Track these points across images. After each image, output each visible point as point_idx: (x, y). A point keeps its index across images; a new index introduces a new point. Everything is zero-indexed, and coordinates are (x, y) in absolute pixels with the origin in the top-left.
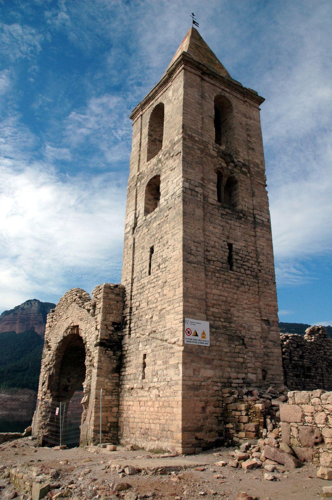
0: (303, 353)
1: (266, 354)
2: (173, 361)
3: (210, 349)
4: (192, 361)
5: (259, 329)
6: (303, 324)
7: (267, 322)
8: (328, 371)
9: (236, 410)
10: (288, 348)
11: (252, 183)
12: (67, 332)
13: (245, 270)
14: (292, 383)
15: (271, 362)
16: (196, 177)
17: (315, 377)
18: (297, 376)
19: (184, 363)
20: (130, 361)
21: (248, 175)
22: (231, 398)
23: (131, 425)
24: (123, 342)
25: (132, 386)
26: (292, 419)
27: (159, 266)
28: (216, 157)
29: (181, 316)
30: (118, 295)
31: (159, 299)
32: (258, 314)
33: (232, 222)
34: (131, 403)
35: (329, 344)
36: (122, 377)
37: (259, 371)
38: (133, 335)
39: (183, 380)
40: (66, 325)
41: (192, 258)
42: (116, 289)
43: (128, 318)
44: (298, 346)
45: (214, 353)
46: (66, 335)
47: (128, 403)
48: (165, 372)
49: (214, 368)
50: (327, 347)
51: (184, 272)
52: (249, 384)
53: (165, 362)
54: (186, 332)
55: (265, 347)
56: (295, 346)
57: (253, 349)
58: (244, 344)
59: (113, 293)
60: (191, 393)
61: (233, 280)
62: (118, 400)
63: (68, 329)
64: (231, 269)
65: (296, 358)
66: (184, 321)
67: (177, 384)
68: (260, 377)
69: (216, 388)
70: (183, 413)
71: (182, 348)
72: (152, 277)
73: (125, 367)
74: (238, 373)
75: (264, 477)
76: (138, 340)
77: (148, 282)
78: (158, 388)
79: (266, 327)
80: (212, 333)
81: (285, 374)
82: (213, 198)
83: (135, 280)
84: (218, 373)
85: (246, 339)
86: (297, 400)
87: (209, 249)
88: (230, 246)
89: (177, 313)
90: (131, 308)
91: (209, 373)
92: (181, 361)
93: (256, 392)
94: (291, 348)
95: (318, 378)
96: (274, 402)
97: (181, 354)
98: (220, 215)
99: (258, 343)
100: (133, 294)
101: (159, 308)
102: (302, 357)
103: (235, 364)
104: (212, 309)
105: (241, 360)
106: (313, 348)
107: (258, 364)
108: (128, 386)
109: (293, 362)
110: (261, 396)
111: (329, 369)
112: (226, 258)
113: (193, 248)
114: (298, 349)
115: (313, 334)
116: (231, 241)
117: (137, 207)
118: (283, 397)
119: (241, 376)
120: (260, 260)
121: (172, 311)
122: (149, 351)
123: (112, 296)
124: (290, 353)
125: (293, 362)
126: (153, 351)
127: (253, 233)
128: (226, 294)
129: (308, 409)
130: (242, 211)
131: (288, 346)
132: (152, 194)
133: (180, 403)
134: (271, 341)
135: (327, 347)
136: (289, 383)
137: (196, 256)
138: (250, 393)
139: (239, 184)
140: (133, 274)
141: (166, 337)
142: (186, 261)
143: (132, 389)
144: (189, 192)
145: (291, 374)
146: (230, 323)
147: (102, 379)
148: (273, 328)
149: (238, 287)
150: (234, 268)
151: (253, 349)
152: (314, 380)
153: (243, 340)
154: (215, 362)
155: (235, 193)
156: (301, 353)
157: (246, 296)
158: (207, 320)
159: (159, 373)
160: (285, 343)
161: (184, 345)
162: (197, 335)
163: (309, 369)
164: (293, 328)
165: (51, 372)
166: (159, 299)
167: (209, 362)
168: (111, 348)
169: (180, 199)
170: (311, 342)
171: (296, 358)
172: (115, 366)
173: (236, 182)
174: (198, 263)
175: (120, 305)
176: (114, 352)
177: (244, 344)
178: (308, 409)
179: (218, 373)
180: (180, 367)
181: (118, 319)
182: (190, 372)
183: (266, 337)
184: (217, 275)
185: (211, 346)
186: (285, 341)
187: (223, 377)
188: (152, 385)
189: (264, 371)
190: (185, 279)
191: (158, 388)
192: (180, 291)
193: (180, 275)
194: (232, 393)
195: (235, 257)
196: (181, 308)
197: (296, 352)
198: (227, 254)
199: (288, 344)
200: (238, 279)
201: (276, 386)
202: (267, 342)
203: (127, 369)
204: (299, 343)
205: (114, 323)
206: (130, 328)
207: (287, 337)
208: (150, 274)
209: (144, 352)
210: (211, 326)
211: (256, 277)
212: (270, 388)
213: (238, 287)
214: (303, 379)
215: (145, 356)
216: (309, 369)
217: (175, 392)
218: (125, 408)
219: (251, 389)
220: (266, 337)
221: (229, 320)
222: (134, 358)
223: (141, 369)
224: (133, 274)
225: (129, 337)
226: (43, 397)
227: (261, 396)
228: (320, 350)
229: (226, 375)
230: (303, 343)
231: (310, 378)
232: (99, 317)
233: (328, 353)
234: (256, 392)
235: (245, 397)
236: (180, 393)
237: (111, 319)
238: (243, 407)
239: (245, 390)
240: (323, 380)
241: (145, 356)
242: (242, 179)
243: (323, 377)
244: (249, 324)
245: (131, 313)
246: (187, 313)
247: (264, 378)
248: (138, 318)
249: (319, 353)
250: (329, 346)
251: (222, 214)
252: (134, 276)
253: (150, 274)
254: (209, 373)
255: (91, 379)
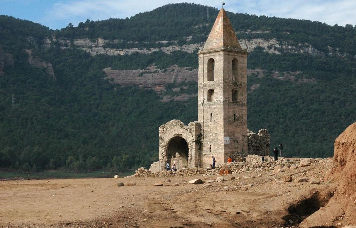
0: (256, 141)
1: (243, 145)
2: (221, 147)
3: (229, 144)
4: (226, 148)
5: (242, 138)
6: (309, 21)
7: (244, 136)
8: (267, 148)
9: (236, 159)
10: (251, 139)
11: (242, 91)
12: (174, 136)
13: (239, 121)
14: (251, 153)
15: (244, 147)
16: (226, 96)
17: (261, 150)
18: (254, 150)
19: (224, 148)
20: (204, 147)
21: (241, 88)
22: (235, 157)
23: (206, 164)
24: (201, 141)
25: (206, 154)
26: (248, 161)
27: (215, 120)
28: (232, 86)
29: (223, 137)
30: (198, 126)
31: (215, 130)
32: (242, 134)
33: (236, 107)
34: (206, 158)
35: (269, 137)
36: (201, 151)
37: (241, 150)
38: (205, 139)
39: (224, 152)
40: (174, 133)
41: (225, 121)
42: (198, 124)
43: (202, 133)
44: (255, 138)
45: (230, 145)
46: (174, 137)
47: (204, 158)
48: (218, 150)
49: (230, 149)
50: (268, 138)
51: (224, 125)
52: (238, 153)
53: (218, 148)
54: (224, 140)
55: (243, 143)
56: (253, 138)
57: (240, 144)
58: (237, 143)
59: (197, 126)
60: (226, 155)
61: (235, 125)
62: (200, 158)
63: (175, 135)
64: (235, 122)
65: (253, 143)
66: (224, 138)
67: (222, 153)
68: (241, 151)
69: (231, 154)
70: (224, 160)
71: (223, 145)
72: (212, 123)
73: (202, 148)
74: (236, 150)
75: (264, 77)
76: (208, 141)
77: (210, 124)
78: (216, 154)
79: (243, 137)
80: (230, 140)
81: (249, 149)
82: (231, 101)
83: (204, 122)
84: (231, 150)
85: (238, 141)
86: (250, 157)
87: (230, 117)
88: (235, 114)
89: (222, 136)
90: (203, 131)
91: (229, 150)
92: (223, 148)
93: (240, 155)
94: (252, 139)
95: (262, 150)
96: (245, 157)
97: (223, 146)
98: (232, 105)
99: (241, 142)
100: (204, 126)
101: (215, 133)
102: (256, 143)
103: (235, 148)
104: (230, 134)
105: (237, 147)
106: (261, 139)
107: (241, 148)
108: (204, 154)
109: (252, 145)
110: (242, 156)
111: (267, 147)
112: (234, 119)
113: (226, 118)
114: (255, 140)
115: (262, 133)
116: (235, 113)
117: (204, 96)
118: (247, 156)
119: (237, 151)
120: (243, 117)
121: (220, 135)
122: (212, 144)
123: (197, 127)
124: (251, 141)
125: (252, 145)
126: (213, 144)
127: (241, 109)
128: (233, 129)
129: (252, 158)
130: (239, 102)
131: (251, 139)
132: (209, 93)
133: (223, 157)
134: (245, 141)
135: (268, 138)
136: (250, 152)
137: (226, 120)
138: (239, 155)
139: (238, 92)
140: (203, 120)
141: (218, 141)
142: (224, 122)
143: (206, 154)
144: (225, 101)
145: (251, 149)
146: (234, 137)
147: (196, 152)
148: (245, 138)
149: (236, 127)
150: (236, 121)
151: (240, 144)
152: (260, 151)
153: (237, 141)
154: (231, 148)
155: (237, 95)
156: (256, 141)
157: (238, 129)
158: (229, 137)
159: (216, 150)
160: (250, 137)
161: (224, 144)
162: (226, 141)
163: (259, 147)
164: (287, 31)
165: (166, 149)
166: (215, 130)
167: (229, 148)
168: (198, 142)
169: (223, 103)
170: (260, 137)
171: (253, 143)
172: (199, 148)
173: (237, 91)
174: (227, 122)
175: (199, 129)
176: (199, 144)
177: (237, 143)
178: (252, 158)
179: (231, 150)
180: (223, 149)
181: (199, 134)
182: (225, 150)
183: (243, 140)
184: (231, 124)
185: (230, 143)
186: (250, 136)
187: (232, 151)
188: (214, 153)
189: (242, 149)
190: (224, 127)
191: (216, 154)
192: (223, 130)
193: (223, 126)
194: (235, 155)
195: (236, 118)
196: (223, 135)
197: (254, 141)
198: (234, 117)
199: (251, 138)
200: (237, 124)
201: (246, 153)
202: (244, 142)
203: (203, 149)
204: (255, 137)
205: (198, 135)
206: (203, 137)
207: (251, 135)
208: (211, 122)
209: (210, 144)
210: (230, 139)
211: (242, 123)
212: (244, 154)
213: (236, 127)
214: (256, 151)
215: (210, 146)
216: (259, 147)
217: (222, 155)
218: (203, 160)
219: (239, 154)
220: (243, 140)
221: (234, 136)
222: (206, 146)
223: (209, 149)
224: (203, 120)
225: (203, 140)
226: (163, 158)
227: (242, 156)
228: (264, 139)
229: (233, 151)
230: (257, 137)
231: (259, 151)
232: (194, 134)
233: (268, 141)
234: (240, 155)
235: (238, 156)
236: (223, 155)
237: (197, 134)
238: (238, 158)
239: (238, 155)
240: (264, 151)
241: (210, 146)
242: (239, 90)
243: (264, 150)
244: (239, 137)
245: (203, 132)
246: (225, 136)
247: (242, 151)
248: (207, 134)
249: (263, 141)
250: (269, 137)
251: (233, 105)
252: (204, 120)
253: (211, 122)
254: (229, 150)
255: (192, 152)
